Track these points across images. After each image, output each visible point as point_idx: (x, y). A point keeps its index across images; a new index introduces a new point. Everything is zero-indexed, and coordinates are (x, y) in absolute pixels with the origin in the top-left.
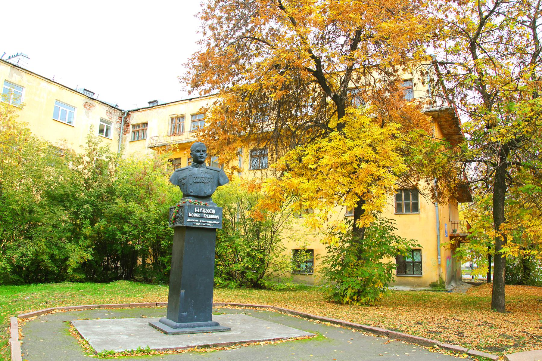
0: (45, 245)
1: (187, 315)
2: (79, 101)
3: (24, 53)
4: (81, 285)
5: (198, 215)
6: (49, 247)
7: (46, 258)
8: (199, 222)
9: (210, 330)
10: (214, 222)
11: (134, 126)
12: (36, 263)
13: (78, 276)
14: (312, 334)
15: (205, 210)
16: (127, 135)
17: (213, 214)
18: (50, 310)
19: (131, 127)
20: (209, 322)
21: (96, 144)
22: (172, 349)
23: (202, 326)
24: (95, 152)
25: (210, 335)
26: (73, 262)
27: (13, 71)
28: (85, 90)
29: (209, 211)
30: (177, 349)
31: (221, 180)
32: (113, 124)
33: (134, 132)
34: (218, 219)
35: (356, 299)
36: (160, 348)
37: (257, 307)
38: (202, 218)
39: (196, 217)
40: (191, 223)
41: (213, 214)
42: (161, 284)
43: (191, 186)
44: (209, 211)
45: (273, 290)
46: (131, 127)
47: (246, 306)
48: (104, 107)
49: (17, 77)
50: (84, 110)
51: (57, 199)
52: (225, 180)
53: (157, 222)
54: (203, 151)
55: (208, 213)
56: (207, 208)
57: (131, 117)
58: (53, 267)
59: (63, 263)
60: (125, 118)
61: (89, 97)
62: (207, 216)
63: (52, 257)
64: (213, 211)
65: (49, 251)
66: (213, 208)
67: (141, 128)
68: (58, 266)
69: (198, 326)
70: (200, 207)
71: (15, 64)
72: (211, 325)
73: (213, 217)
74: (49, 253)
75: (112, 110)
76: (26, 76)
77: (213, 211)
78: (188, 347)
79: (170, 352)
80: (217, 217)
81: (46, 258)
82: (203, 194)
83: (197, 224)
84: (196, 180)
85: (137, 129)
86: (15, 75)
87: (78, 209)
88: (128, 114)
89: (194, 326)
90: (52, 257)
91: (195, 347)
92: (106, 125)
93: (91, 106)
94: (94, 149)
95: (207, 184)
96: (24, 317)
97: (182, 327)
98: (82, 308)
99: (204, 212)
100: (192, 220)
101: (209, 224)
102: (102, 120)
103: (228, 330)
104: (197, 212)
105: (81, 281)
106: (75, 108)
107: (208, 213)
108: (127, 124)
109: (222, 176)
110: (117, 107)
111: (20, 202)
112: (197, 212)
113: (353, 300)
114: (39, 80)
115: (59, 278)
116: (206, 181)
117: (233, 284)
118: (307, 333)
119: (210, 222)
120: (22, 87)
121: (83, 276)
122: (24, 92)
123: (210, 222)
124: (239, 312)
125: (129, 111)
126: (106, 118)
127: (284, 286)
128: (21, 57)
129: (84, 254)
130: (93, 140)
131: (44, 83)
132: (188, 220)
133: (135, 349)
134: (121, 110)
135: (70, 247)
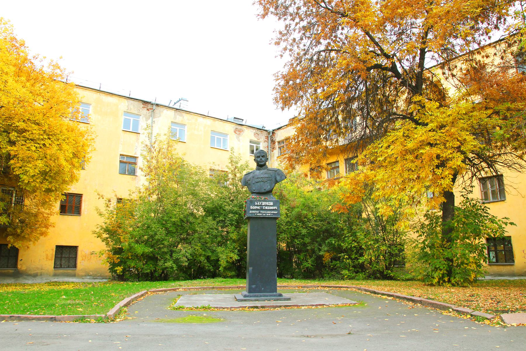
0: (201, 249)
1: (256, 287)
2: (229, 128)
3: (184, 98)
5: (259, 208)
6: (204, 250)
7: (202, 259)
8: (259, 213)
11: (279, 142)
12: (193, 261)
13: (230, 274)
14: (354, 302)
15: (264, 203)
16: (275, 151)
17: (271, 206)
18: (176, 289)
19: (277, 143)
20: (275, 293)
21: (237, 163)
22: (228, 308)
24: (237, 170)
26: (223, 263)
27: (176, 114)
28: (235, 118)
29: (267, 203)
30: (232, 308)
31: (278, 178)
32: (261, 144)
33: (280, 148)
35: (446, 280)
36: (218, 306)
37: (342, 287)
38: (262, 209)
39: (257, 210)
41: (271, 206)
42: (300, 279)
43: (254, 185)
44: (267, 203)
45: (399, 280)
46: (277, 143)
47: (334, 287)
48: (252, 130)
49: (180, 118)
50: (235, 136)
51: (213, 211)
52: (281, 177)
53: (289, 223)
54: (262, 156)
55: (267, 206)
56: (266, 201)
57: (276, 135)
58: (208, 266)
59: (216, 263)
60: (271, 137)
61: (239, 124)
62: (266, 208)
63: (208, 258)
64: (272, 204)
65: (204, 253)
66: (271, 201)
67: (285, 144)
68: (213, 266)
70: (260, 201)
71: (178, 108)
72: (275, 296)
73: (272, 208)
74: (205, 255)
75: (259, 132)
76: (186, 116)
77: (272, 204)
78: (241, 307)
79: (225, 310)
80: (275, 208)
81: (202, 259)
82: (263, 191)
84: (257, 180)
85: (282, 145)
86: (178, 116)
87: (225, 219)
88: (273, 133)
89: (261, 296)
90: (208, 258)
91: (246, 307)
92: (255, 145)
93: (240, 131)
94: (236, 168)
96: (154, 292)
98: (200, 288)
101: (269, 214)
102: (251, 142)
103: (289, 299)
104: (257, 205)
105: (232, 277)
106: (227, 135)
107: (267, 206)
108: (273, 142)
109: (279, 175)
110: (264, 129)
111: (177, 215)
113: (444, 281)
115: (214, 275)
116: (265, 180)
117: (361, 275)
118: (348, 301)
120: (184, 125)
121: (233, 273)
124: (321, 291)
125: (274, 130)
126: (255, 139)
127: (409, 276)
128: (182, 101)
129: (232, 255)
130: (234, 160)
131: (200, 119)
132: (250, 212)
133: (199, 306)
134: (266, 131)
135: (220, 249)
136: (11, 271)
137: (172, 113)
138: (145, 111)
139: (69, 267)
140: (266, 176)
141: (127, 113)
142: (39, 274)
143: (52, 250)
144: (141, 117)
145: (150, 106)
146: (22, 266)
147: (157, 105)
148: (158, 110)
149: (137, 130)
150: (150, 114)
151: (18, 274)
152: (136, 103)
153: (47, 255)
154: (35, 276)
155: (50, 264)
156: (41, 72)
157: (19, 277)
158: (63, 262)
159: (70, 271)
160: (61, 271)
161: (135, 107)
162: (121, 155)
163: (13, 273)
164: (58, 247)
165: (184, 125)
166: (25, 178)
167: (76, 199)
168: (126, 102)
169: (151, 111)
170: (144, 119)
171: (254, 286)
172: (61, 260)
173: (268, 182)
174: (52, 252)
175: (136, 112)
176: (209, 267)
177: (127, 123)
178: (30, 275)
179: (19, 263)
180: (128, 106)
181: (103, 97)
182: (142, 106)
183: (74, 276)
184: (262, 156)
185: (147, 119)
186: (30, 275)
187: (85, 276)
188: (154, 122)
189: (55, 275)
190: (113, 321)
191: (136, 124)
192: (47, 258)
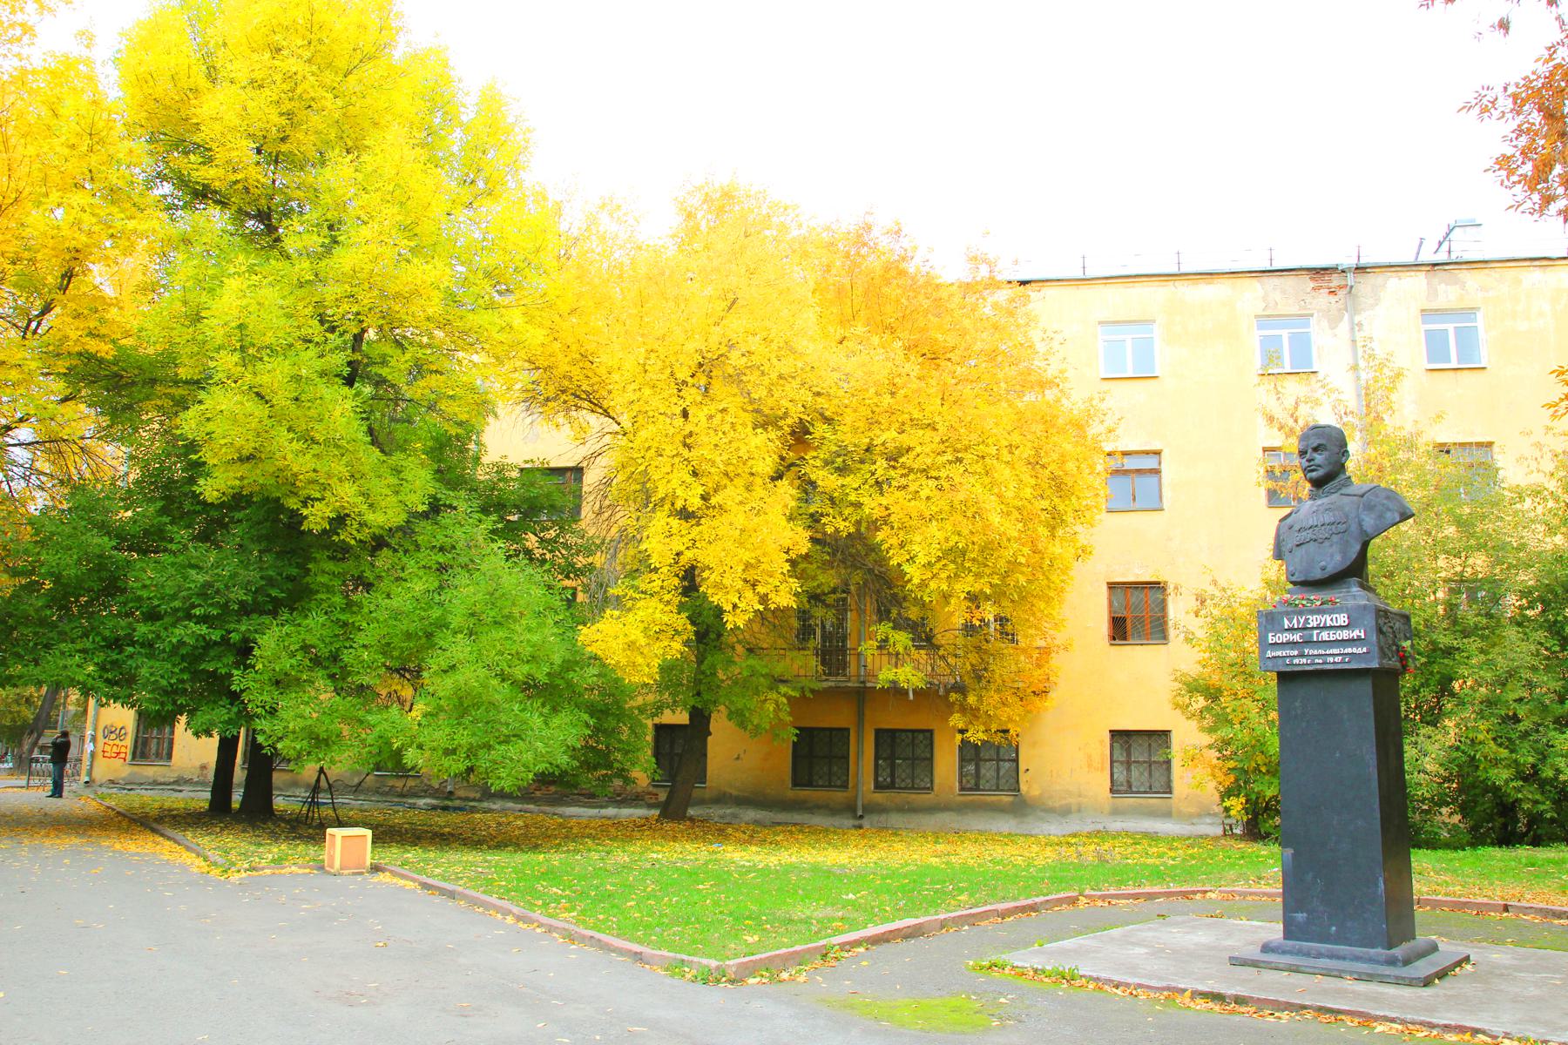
4: (1450, 854)
5: (1296, 637)
8: (1301, 655)
9: (1351, 973)
10: (1349, 650)
15: (1314, 621)
23: (1344, 958)
25: (1348, 984)
27: (1435, 281)
29: (1327, 619)
34: (1359, 639)
38: (1308, 642)
40: (1280, 661)
49: (1448, 292)
55: (1325, 628)
62: (1325, 636)
64: (1342, 619)
66: (1340, 611)
69: (1332, 956)
70: (1301, 613)
73: (1345, 634)
76: (1472, 279)
77: (1342, 619)
80: (1355, 633)
82: (1317, 575)
83: (1296, 661)
89: (1319, 955)
91: (1184, 991)
95: (1327, 543)
97: (1284, 952)
99: (1313, 624)
100: (1279, 653)
104: (1291, 629)
107: (1325, 628)
112: (1291, 629)
114: (1511, 273)
119: (1336, 651)
120: (1469, 312)
122: (1480, 322)
123: (1336, 651)
131: (1533, 276)
136: (1006, 799)
137: (1418, 280)
138: (1323, 299)
139: (1150, 790)
140: (1328, 518)
141: (1264, 320)
142: (1074, 808)
143: (1102, 742)
144: (1313, 321)
145: (1336, 280)
146: (1029, 786)
147: (1360, 269)
148: (1365, 284)
149: (1310, 365)
150: (1340, 305)
151: (1021, 807)
152: (1289, 281)
153: (1089, 757)
154: (1065, 812)
155: (1097, 783)
156: (87, 507)
157: (1024, 815)
158: (1135, 773)
159: (1154, 802)
160: (1129, 801)
161: (1285, 296)
162: (1265, 450)
163: (1012, 803)
164: (1115, 734)
165: (1469, 312)
166: (914, 573)
167: (1155, 596)
168: (1254, 287)
169: (1342, 293)
170: (1325, 324)
171: (1300, 916)
172: (1129, 770)
173: (1335, 538)
174: (1101, 748)
175: (1294, 310)
176: (1536, 802)
177: (1271, 354)
178: (1051, 811)
179: (1023, 777)
180: (1264, 299)
181: (1184, 290)
182: (1312, 285)
183: (1167, 814)
184: (1315, 449)
185: (1334, 323)
186: (1051, 811)
187: (1199, 815)
188: (1360, 324)
189: (1116, 812)
190: (732, 982)
191: (1302, 345)
192: (1089, 766)
